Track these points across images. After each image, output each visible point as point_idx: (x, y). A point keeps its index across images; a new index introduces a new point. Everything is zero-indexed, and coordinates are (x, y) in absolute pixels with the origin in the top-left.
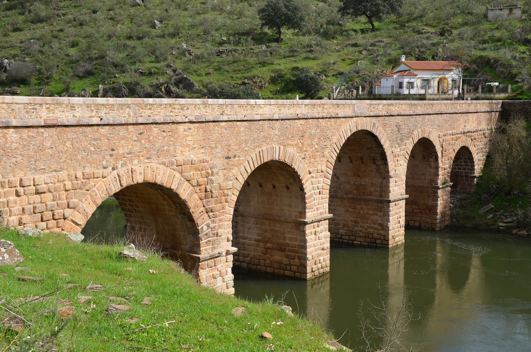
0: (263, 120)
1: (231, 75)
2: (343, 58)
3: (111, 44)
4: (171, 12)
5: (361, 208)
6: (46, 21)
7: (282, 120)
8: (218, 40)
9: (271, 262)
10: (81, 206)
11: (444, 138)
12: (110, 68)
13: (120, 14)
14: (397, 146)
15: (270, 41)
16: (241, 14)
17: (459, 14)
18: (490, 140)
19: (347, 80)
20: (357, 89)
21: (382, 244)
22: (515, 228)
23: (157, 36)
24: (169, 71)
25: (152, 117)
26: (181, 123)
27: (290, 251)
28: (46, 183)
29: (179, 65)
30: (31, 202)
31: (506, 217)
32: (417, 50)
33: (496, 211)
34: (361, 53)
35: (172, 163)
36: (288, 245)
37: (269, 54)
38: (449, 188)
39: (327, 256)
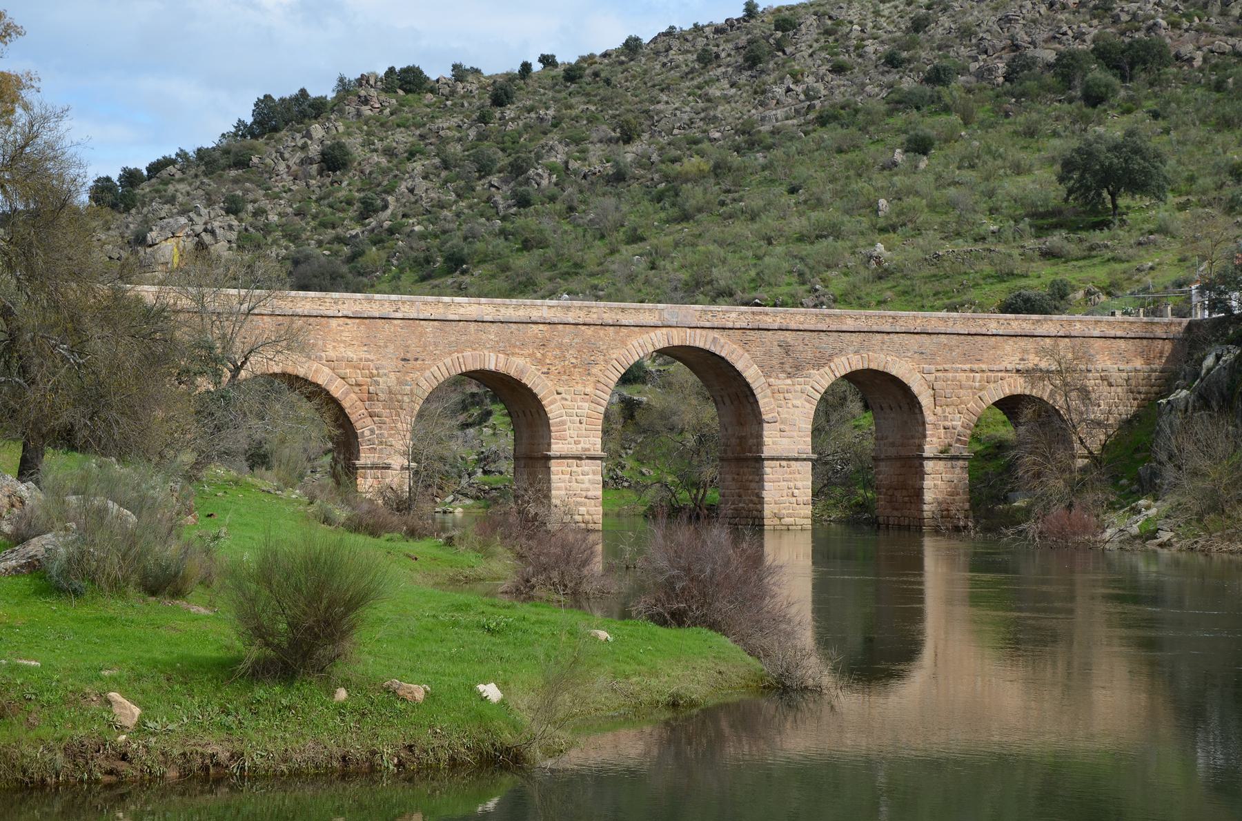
7: (502, 322)
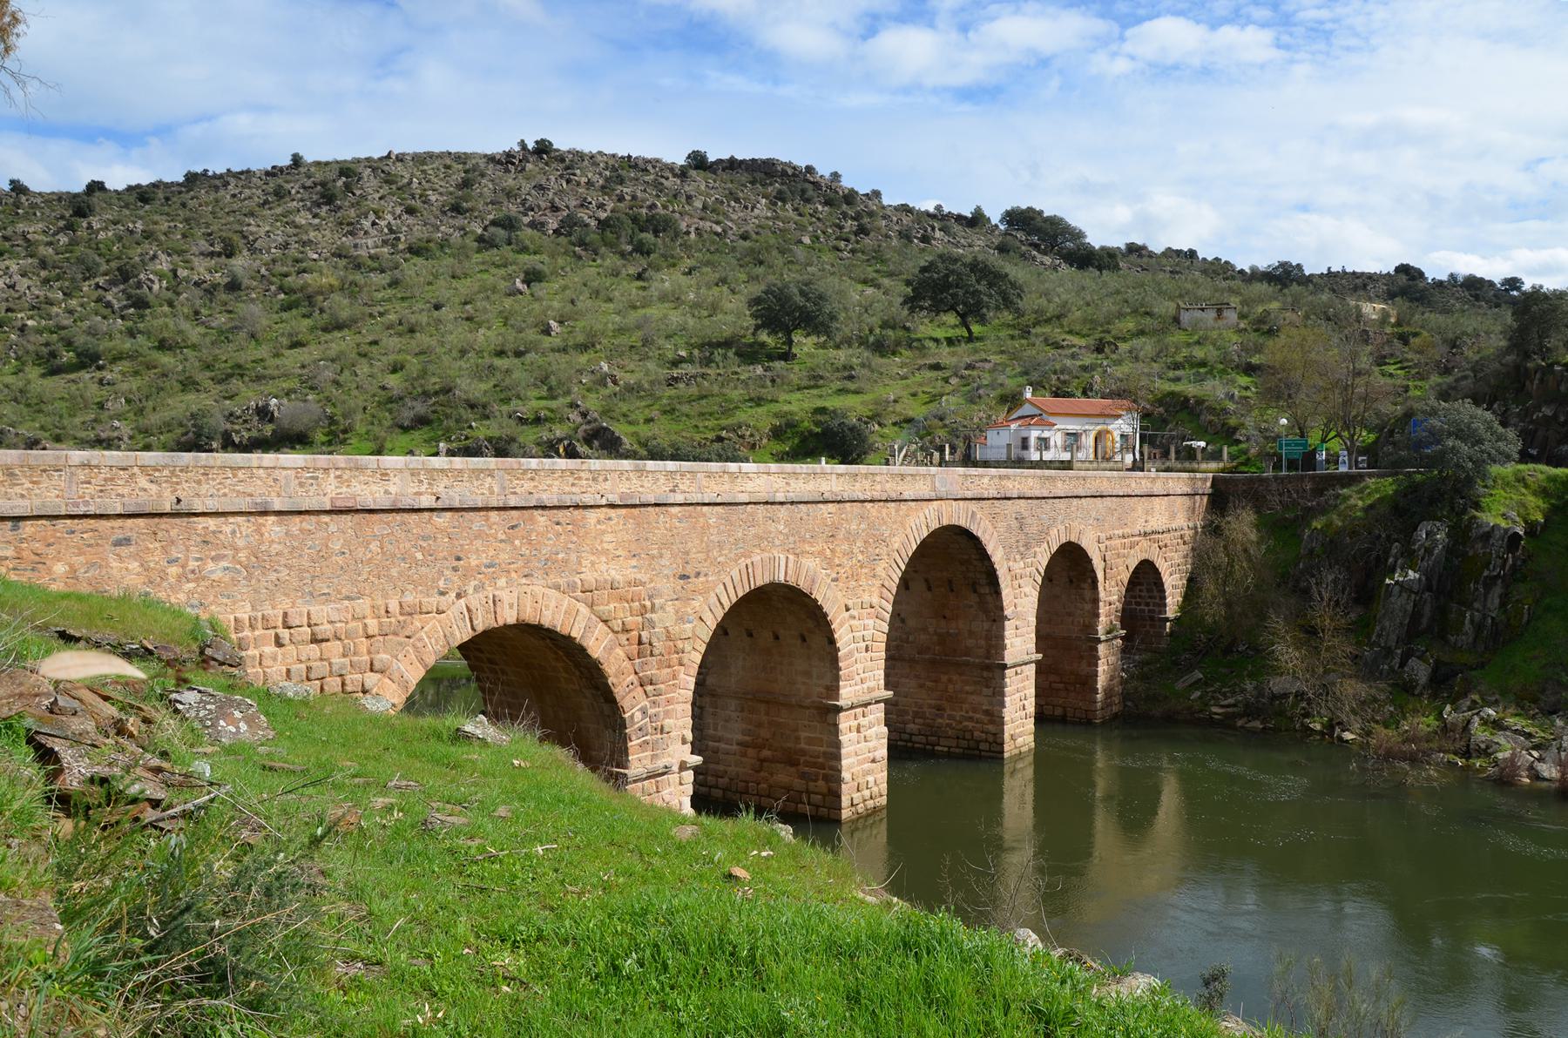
0: (755, 503)
1: (694, 422)
2: (912, 391)
3: (464, 366)
4: (579, 305)
5: (950, 681)
6: (349, 327)
7: (792, 503)
8: (670, 355)
9: (770, 786)
10: (395, 667)
11: (1108, 543)
12: (462, 411)
13: (485, 311)
14: (1018, 557)
15: (771, 358)
16: (714, 308)
17: (1129, 314)
18: (1193, 549)
19: (921, 432)
20: (941, 450)
21: (990, 751)
22: (1241, 716)
23: (553, 350)
24: (575, 416)
25: (536, 496)
26: (591, 507)
27: (807, 764)
28: (331, 622)
29: (593, 403)
30: (303, 659)
31: (1224, 695)
32: (1054, 377)
33: (1206, 684)
34: (947, 382)
35: (572, 587)
36: (803, 753)
37: (769, 383)
38: (1120, 641)
39: (882, 775)
